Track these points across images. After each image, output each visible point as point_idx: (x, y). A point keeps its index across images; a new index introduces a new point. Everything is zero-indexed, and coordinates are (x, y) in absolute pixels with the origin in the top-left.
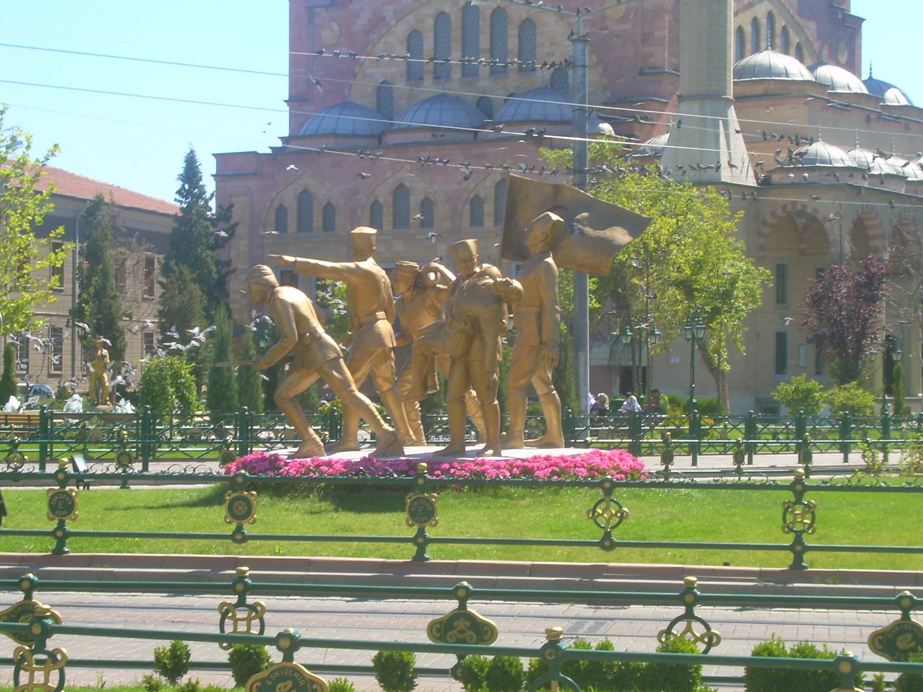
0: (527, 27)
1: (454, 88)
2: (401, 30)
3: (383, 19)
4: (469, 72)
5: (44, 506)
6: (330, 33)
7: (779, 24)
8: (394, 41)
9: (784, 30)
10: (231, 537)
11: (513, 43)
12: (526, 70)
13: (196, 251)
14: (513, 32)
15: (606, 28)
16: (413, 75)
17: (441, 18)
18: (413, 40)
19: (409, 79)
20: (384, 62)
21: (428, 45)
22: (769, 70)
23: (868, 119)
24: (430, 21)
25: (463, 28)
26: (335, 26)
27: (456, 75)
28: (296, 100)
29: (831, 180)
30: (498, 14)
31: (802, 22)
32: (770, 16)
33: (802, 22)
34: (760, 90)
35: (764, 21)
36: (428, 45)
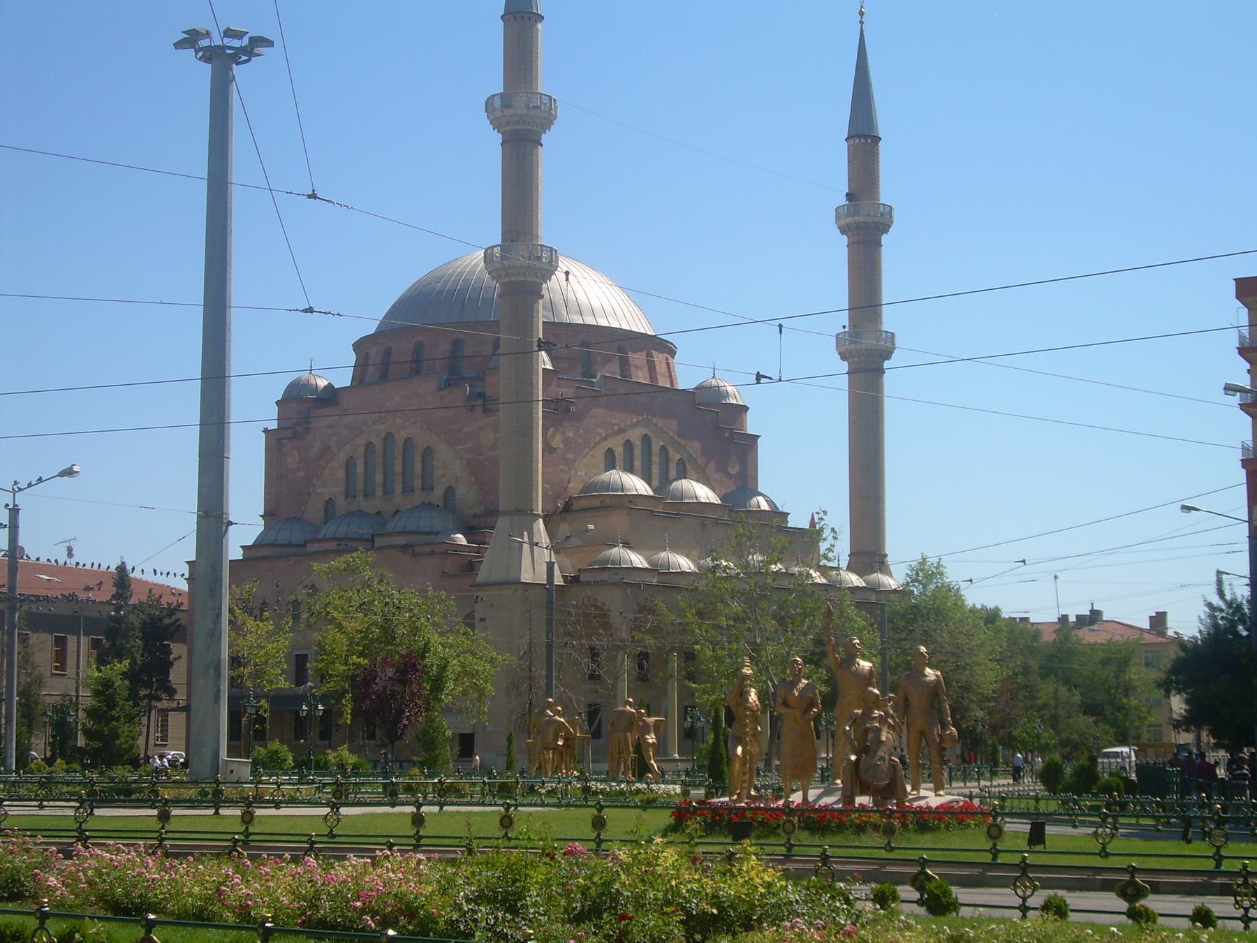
0: (428, 453)
1: (361, 503)
2: (342, 457)
3: (329, 448)
4: (388, 491)
5: (609, 824)
6: (292, 461)
7: (656, 446)
8: (336, 469)
9: (664, 449)
10: (1099, 854)
11: (418, 467)
12: (427, 487)
13: (137, 635)
14: (418, 458)
15: (480, 454)
16: (349, 494)
17: (369, 445)
18: (350, 464)
19: (347, 497)
20: (330, 485)
21: (360, 469)
22: (607, 486)
23: (703, 525)
24: (362, 449)
25: (384, 454)
26: (296, 455)
27: (379, 493)
28: (268, 515)
29: (617, 579)
30: (408, 441)
31: (683, 442)
32: (646, 439)
33: (683, 442)
34: (597, 503)
35: (638, 443)
36: (360, 469)
